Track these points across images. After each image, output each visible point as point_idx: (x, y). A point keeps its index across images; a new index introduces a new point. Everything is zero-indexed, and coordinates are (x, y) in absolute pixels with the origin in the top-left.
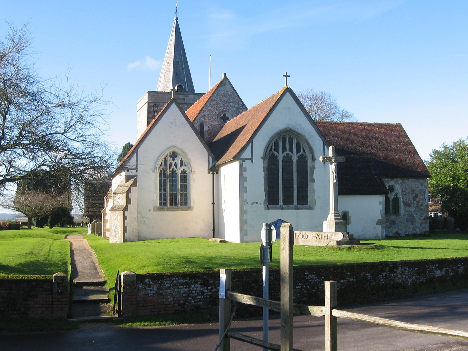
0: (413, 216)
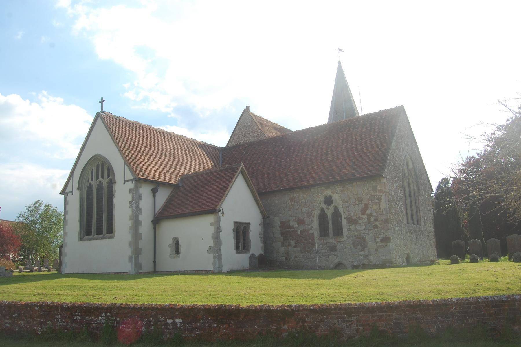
0: (363, 238)
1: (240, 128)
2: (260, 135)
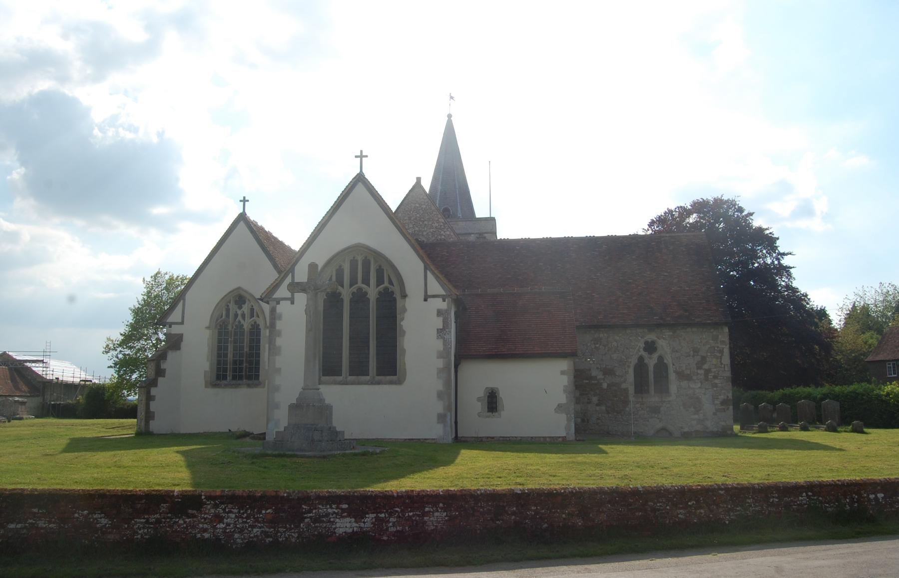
1: (407, 209)
2: (443, 227)
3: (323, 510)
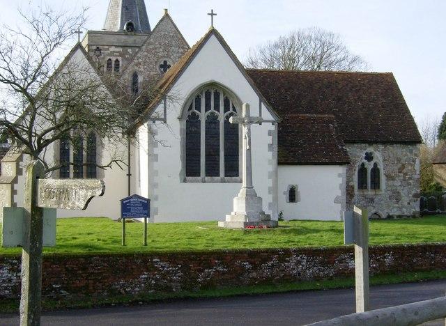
3: (343, 256)
